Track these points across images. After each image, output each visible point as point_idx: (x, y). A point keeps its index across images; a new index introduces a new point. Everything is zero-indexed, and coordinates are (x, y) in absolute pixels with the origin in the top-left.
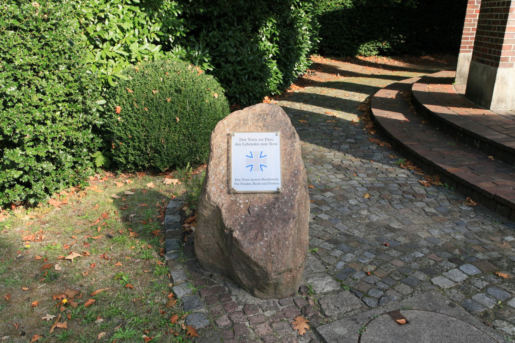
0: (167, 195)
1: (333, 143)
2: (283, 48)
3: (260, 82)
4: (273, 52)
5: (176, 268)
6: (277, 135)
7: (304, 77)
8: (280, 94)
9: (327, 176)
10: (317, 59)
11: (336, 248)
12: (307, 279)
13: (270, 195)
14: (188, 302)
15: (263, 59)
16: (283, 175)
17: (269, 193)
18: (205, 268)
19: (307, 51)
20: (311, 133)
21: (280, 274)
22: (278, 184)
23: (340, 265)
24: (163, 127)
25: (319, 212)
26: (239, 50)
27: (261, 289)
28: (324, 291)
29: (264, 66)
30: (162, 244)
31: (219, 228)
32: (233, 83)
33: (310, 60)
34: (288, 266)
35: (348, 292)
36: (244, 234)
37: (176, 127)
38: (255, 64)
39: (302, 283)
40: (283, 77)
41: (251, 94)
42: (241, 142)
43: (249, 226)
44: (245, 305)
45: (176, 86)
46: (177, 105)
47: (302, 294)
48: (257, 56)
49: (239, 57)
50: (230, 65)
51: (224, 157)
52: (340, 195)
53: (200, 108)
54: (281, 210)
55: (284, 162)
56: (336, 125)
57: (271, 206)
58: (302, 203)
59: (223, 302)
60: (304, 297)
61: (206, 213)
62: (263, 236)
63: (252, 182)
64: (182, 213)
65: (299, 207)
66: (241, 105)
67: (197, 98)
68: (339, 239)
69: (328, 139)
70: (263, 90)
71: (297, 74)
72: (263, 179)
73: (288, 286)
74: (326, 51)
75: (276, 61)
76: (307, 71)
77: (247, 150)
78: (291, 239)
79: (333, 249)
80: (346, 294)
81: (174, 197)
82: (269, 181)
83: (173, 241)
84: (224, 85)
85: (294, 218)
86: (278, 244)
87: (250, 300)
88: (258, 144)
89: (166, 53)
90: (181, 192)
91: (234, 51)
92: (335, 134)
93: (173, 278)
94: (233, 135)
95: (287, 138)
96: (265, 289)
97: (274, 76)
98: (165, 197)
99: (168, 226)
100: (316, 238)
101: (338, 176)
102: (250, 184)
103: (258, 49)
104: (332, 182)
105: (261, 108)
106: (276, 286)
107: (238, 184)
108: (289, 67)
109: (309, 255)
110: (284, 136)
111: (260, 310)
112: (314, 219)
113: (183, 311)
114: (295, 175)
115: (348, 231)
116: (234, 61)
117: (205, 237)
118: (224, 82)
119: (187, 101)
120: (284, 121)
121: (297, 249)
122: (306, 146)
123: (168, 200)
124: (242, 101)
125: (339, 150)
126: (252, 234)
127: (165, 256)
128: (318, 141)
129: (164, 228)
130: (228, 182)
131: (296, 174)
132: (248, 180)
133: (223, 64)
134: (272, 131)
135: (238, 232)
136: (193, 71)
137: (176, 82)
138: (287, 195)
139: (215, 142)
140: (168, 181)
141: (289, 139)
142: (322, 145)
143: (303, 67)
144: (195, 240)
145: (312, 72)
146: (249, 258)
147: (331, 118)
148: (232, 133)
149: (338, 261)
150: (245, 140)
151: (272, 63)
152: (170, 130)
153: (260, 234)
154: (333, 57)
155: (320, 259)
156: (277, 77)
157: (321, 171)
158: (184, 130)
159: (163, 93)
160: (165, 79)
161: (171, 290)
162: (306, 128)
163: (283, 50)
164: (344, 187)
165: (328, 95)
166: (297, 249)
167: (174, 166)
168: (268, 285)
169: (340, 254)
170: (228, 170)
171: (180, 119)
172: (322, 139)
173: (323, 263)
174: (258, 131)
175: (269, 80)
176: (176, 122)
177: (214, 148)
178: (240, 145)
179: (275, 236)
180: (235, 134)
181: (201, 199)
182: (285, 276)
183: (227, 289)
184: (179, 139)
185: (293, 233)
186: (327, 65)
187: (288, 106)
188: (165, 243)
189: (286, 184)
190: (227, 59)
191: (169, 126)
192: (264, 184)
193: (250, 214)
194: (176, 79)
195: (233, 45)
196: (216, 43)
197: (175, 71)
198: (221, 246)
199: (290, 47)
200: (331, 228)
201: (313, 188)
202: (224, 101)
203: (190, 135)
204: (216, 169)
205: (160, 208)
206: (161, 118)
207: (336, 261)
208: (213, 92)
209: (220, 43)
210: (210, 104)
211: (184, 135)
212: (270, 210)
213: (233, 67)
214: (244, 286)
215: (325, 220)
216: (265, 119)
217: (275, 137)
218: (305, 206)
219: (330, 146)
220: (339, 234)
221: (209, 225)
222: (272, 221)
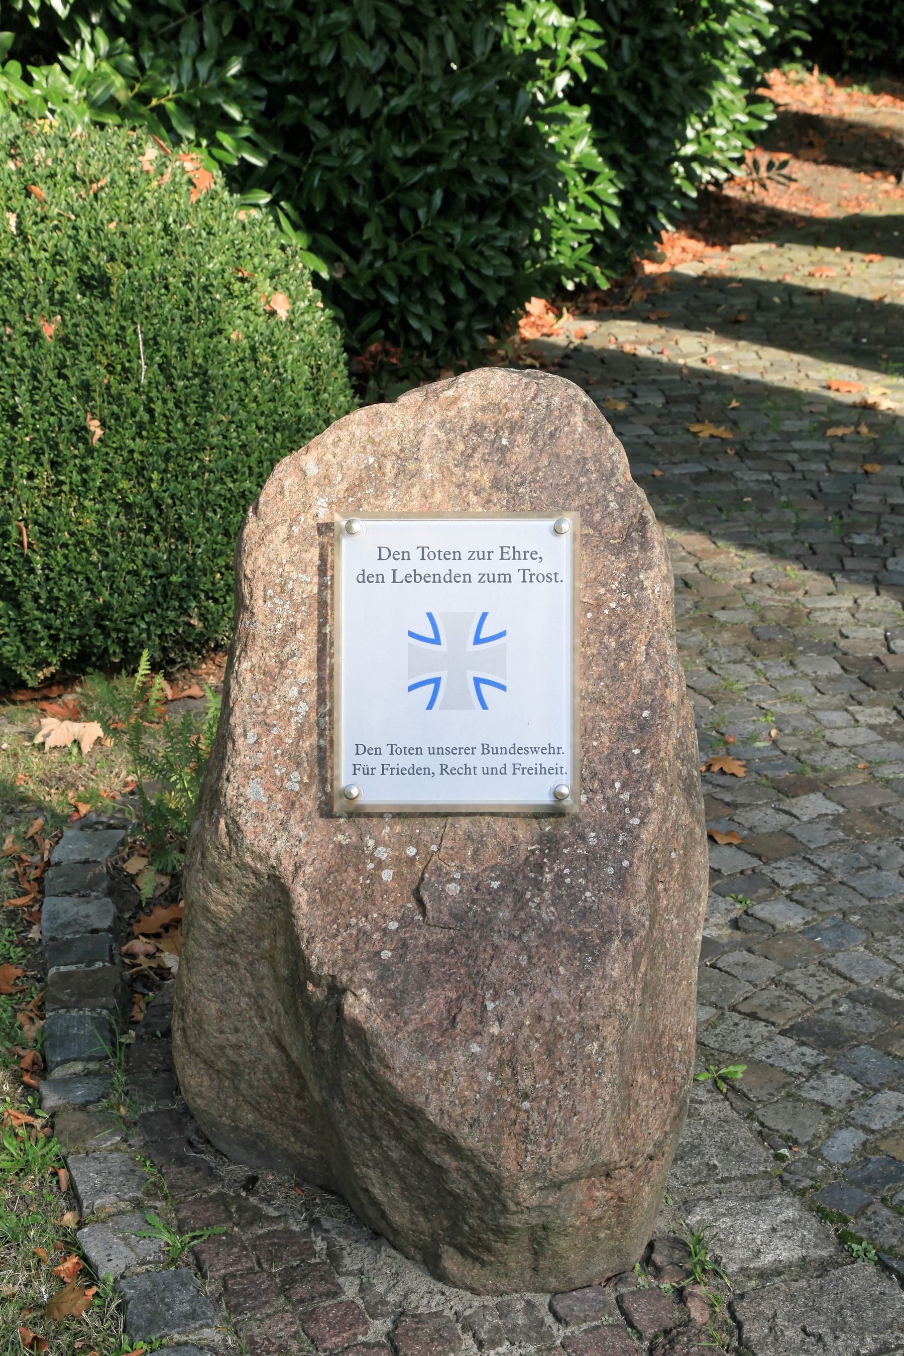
0: (53, 798)
1: (851, 547)
2: (626, 41)
3: (503, 224)
4: (576, 61)
5: (92, 1143)
6: (557, 531)
7: (730, 191)
8: (604, 285)
9: (810, 713)
10: (803, 90)
11: (828, 1065)
12: (687, 1206)
13: (518, 821)
14: (147, 1296)
15: (523, 99)
16: (585, 730)
17: (516, 815)
18: (223, 1146)
19: (749, 52)
20: (748, 492)
21: (557, 1186)
22: (558, 771)
23: (846, 1142)
24: (25, 469)
25: (762, 891)
26: (402, 58)
27: (474, 1249)
28: (758, 1264)
29: (527, 140)
30: (31, 1031)
31: (284, 972)
32: (369, 231)
33: (761, 100)
34: (595, 1154)
35: (871, 1269)
36: (394, 1007)
37: (84, 470)
38: (482, 129)
39: (662, 1225)
40: (620, 195)
41: (459, 290)
42: (385, 568)
43: (417, 970)
44: (399, 1317)
45: (85, 259)
46: (92, 358)
47: (658, 1272)
48: (490, 85)
49: (401, 90)
50: (355, 134)
51: (306, 640)
52: (868, 812)
53: (203, 373)
54: (568, 898)
55: (588, 666)
56: (876, 454)
57: (522, 877)
58: (669, 863)
59: (302, 1301)
60: (666, 1285)
61: (223, 902)
62: (482, 1016)
63: (434, 762)
64: (120, 886)
65: (652, 881)
66: (408, 344)
67: (188, 320)
68: (845, 1022)
69: (827, 525)
70: (518, 265)
71: (691, 176)
72: (486, 749)
73: (596, 1238)
74: (852, 44)
75: (586, 111)
76: (749, 157)
77: (415, 604)
78: (610, 1030)
79: (814, 1069)
80: (862, 1277)
81: (84, 809)
82: (516, 758)
83: (81, 1021)
84: (326, 243)
85: (629, 933)
86: (550, 1050)
87: (422, 1293)
88: (467, 578)
89: (36, 74)
90: (117, 784)
91: (373, 61)
92: (867, 498)
93: (81, 1188)
94: (349, 531)
95: (607, 545)
96: (489, 1250)
97: (578, 190)
98: (40, 808)
99: (59, 949)
100: (736, 1017)
101: (865, 715)
102: (427, 771)
103: (496, 48)
104: (832, 745)
105: (484, 390)
106: (540, 1239)
108: (653, 143)
109: (702, 1095)
110: (593, 540)
111: (468, 1340)
112: (735, 924)
113: (125, 1339)
114: (641, 729)
115: (891, 984)
116: (377, 114)
117: (222, 1013)
118: (326, 225)
119: (137, 335)
120: (597, 459)
121: (641, 1078)
122: (721, 559)
123: (59, 821)
124: (415, 324)
125: (878, 584)
126: (433, 1003)
127: (45, 1090)
128: (777, 537)
129: (39, 957)
130: (324, 757)
131: (643, 726)
132: (418, 751)
133: (320, 131)
134: (536, 511)
135: (366, 998)
136: (167, 178)
137: (83, 237)
138: (598, 826)
139: (261, 562)
140: (57, 730)
141: (617, 551)
142: (797, 558)
143: (724, 141)
144: (176, 1024)
145: (770, 166)
146: (414, 1114)
147: (855, 414)
148: (340, 521)
149: (834, 1127)
151: (564, 120)
152: (59, 483)
153: (467, 1007)
154: (885, 80)
155: (750, 1116)
156: (592, 194)
157: (783, 690)
158: (124, 484)
159: (19, 292)
160: (28, 222)
161: (71, 1245)
162: (723, 466)
163: (626, 52)
164: (887, 772)
165: (846, 290)
166: (641, 1078)
167: (87, 658)
168: (503, 1233)
169: (846, 1095)
170: (321, 699)
171: (103, 425)
172: (798, 527)
173: (764, 1135)
174: (465, 513)
175: (549, 213)
176: (86, 442)
177: (258, 594)
178: (380, 578)
179: (540, 1018)
180: (356, 526)
181: (200, 837)
182: (580, 1196)
183: (320, 1245)
184: (101, 526)
185: (622, 1005)
186: (852, 126)
187: (643, 351)
188: (42, 1031)
190: (340, 104)
191: (53, 464)
192: (493, 771)
193: (424, 913)
194: (82, 223)
195: (369, 25)
196: (282, 20)
197: (75, 177)
198: (294, 1055)
199: (659, 33)
200: (812, 968)
201: (740, 772)
202: (320, 331)
203: (158, 505)
204: (264, 693)
205: (20, 860)
206: (14, 424)
207: (822, 1127)
208: (266, 286)
209: (303, 20)
210: (253, 349)
211: (128, 507)
212: (519, 896)
213: (370, 148)
214: (396, 1232)
215: (789, 933)
216: (503, 450)
217: (550, 543)
218: (685, 879)
219: (836, 561)
220: (851, 997)
221: (237, 958)
222: (525, 948)
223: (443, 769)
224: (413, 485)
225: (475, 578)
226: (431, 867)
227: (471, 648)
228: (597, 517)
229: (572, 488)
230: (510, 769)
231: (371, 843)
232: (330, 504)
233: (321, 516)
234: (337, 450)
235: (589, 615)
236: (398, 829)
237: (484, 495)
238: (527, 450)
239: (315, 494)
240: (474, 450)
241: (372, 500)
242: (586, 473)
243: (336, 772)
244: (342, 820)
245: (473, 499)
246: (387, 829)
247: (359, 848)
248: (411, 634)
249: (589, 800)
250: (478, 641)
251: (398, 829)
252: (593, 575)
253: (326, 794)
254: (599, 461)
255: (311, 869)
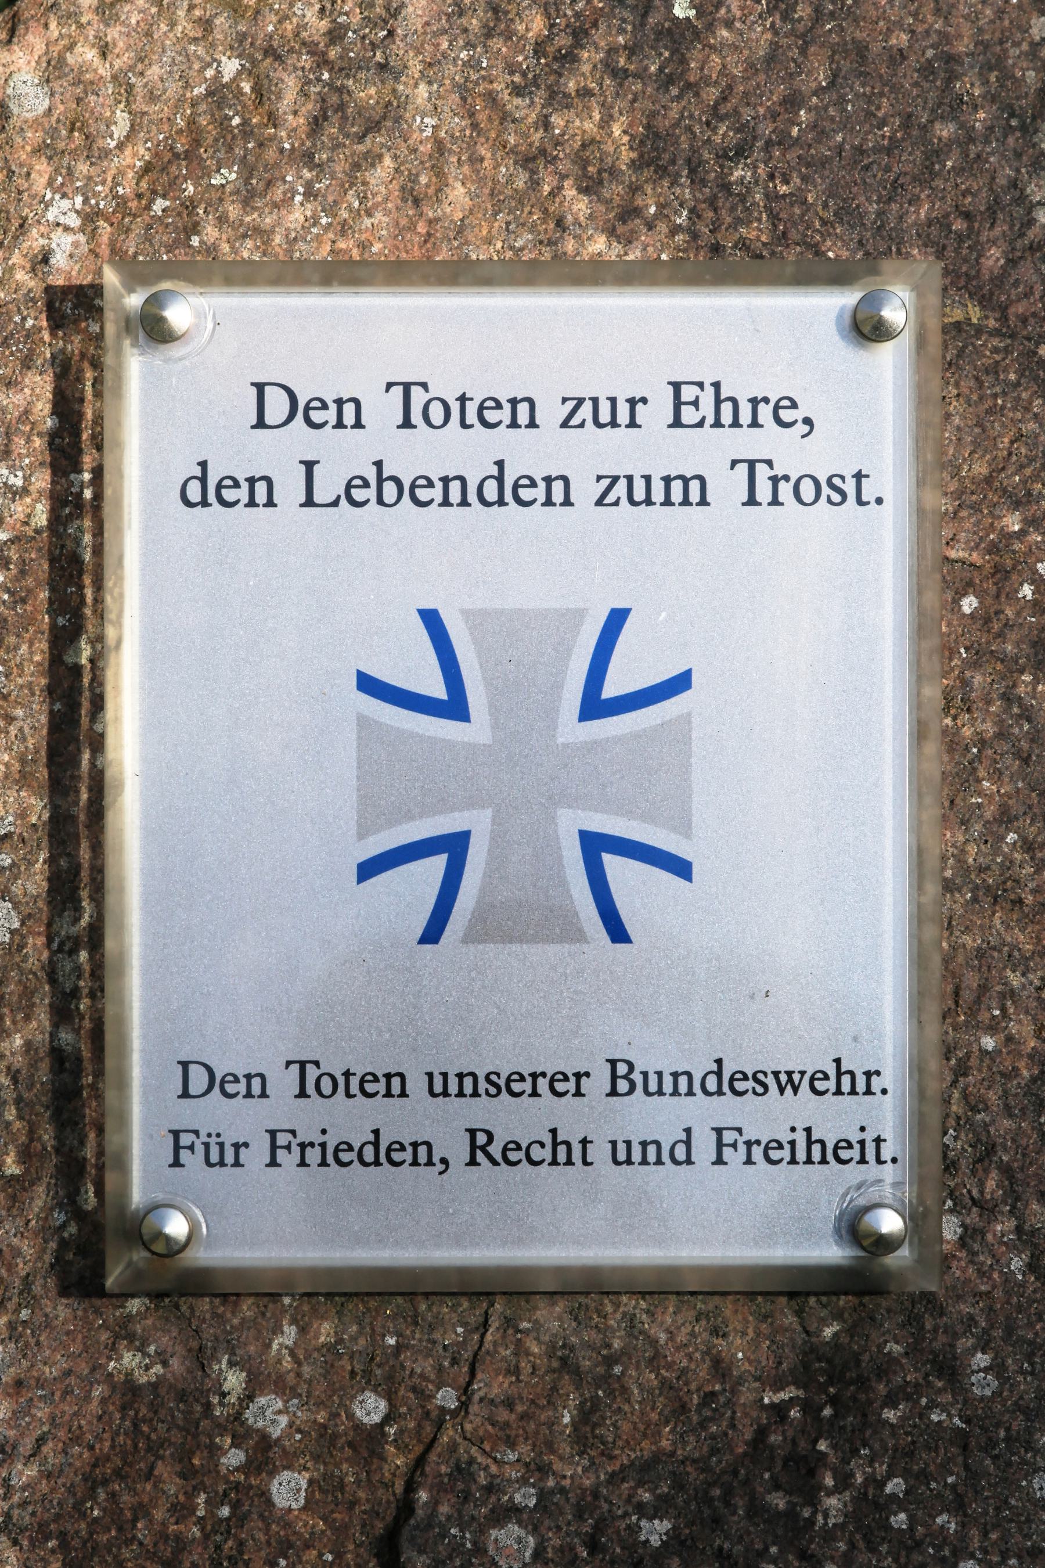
22: (865, 1150)
42: (279, 453)
63: (445, 1125)
72: (622, 1078)
82: (726, 1110)
88: (557, 492)
94: (154, 329)
102: (421, 1154)
107: (225, 1155)
130: (74, 1085)
132: (394, 1086)
150: (348, 413)
178: (260, 490)
180: (178, 315)
189: (986, 1152)
223: (479, 1146)
224: (373, 159)
225: (585, 491)
226: (439, 1466)
227: (572, 730)
228: (994, 257)
229: (910, 160)
230: (704, 1147)
231: (234, 1381)
232: (90, 218)
233: (59, 260)
234: (113, 33)
235: (969, 604)
236: (325, 1331)
237: (615, 191)
238: (760, 37)
239: (39, 182)
240: (580, 34)
241: (233, 211)
242: (954, 107)
243: (112, 1140)
244: (135, 1305)
245: (578, 206)
246: (289, 1334)
247: (194, 1395)
248: (368, 684)
249: (968, 1236)
250: (594, 706)
251: (325, 1331)
252: (981, 469)
253: (78, 1215)
254: (998, 64)
255: (32, 1471)
